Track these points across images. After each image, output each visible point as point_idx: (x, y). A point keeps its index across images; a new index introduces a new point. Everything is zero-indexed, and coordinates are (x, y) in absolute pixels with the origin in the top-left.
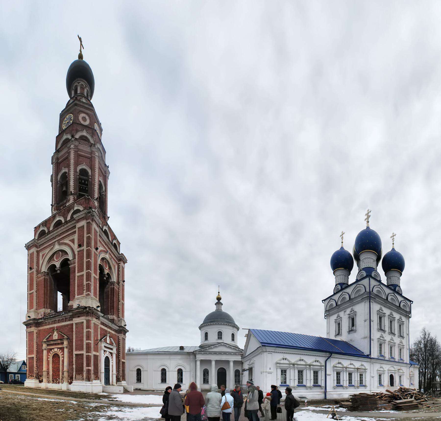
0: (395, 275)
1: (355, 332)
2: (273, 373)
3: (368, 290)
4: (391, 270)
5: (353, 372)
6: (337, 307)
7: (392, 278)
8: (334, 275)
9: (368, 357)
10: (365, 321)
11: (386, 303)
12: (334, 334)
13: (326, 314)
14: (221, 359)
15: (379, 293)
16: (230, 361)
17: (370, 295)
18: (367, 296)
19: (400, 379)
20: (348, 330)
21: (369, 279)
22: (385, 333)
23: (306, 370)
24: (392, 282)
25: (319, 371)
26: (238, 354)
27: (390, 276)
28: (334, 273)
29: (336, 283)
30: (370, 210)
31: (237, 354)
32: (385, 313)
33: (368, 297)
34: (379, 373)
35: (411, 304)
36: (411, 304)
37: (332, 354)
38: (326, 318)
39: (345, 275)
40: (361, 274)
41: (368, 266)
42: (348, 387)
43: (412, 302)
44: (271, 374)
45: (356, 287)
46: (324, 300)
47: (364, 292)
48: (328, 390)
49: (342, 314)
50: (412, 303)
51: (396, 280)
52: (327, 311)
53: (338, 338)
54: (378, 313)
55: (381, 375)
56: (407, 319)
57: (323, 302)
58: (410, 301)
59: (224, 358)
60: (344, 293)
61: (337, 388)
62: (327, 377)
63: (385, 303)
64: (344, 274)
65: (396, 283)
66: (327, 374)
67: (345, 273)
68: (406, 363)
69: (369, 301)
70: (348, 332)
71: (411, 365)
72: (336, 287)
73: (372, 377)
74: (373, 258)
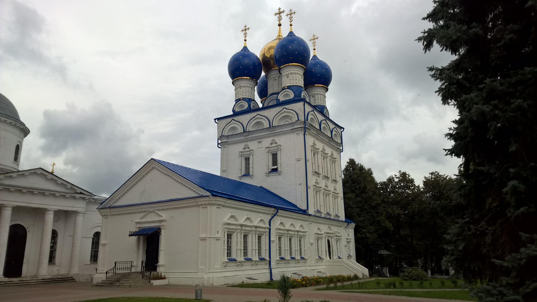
0: (318, 93)
1: (280, 174)
3: (302, 118)
4: (315, 86)
5: (293, 237)
6: (245, 134)
7: (316, 96)
8: (233, 86)
9: (304, 212)
10: (299, 160)
11: (318, 134)
13: (220, 142)
14: (29, 205)
15: (312, 122)
16: (49, 210)
17: (305, 126)
18: (300, 126)
19: (228, 241)
21: (304, 105)
22: (319, 177)
24: (317, 101)
25: (249, 235)
26: (70, 196)
27: (313, 93)
28: (233, 83)
29: (236, 97)
30: (316, 36)
31: (68, 196)
32: (328, 153)
33: (303, 129)
34: (278, 234)
35: (342, 132)
36: (342, 132)
37: (278, 210)
39: (252, 87)
43: (343, 129)
44: (205, 241)
45: (282, 112)
46: (219, 119)
47: (296, 121)
48: (272, 267)
49: (252, 145)
50: (342, 130)
51: (322, 99)
52: (224, 136)
53: (246, 180)
54: (312, 150)
55: (231, 235)
56: (338, 154)
57: (216, 121)
58: (341, 128)
59: (36, 202)
60: (258, 116)
61: (261, 263)
62: (271, 243)
63: (317, 134)
64: (251, 86)
65: (322, 103)
66: (271, 240)
67: (253, 85)
68: (341, 221)
69: (303, 133)
71: (347, 224)
72: (237, 104)
73: (201, 240)
74: (299, 73)
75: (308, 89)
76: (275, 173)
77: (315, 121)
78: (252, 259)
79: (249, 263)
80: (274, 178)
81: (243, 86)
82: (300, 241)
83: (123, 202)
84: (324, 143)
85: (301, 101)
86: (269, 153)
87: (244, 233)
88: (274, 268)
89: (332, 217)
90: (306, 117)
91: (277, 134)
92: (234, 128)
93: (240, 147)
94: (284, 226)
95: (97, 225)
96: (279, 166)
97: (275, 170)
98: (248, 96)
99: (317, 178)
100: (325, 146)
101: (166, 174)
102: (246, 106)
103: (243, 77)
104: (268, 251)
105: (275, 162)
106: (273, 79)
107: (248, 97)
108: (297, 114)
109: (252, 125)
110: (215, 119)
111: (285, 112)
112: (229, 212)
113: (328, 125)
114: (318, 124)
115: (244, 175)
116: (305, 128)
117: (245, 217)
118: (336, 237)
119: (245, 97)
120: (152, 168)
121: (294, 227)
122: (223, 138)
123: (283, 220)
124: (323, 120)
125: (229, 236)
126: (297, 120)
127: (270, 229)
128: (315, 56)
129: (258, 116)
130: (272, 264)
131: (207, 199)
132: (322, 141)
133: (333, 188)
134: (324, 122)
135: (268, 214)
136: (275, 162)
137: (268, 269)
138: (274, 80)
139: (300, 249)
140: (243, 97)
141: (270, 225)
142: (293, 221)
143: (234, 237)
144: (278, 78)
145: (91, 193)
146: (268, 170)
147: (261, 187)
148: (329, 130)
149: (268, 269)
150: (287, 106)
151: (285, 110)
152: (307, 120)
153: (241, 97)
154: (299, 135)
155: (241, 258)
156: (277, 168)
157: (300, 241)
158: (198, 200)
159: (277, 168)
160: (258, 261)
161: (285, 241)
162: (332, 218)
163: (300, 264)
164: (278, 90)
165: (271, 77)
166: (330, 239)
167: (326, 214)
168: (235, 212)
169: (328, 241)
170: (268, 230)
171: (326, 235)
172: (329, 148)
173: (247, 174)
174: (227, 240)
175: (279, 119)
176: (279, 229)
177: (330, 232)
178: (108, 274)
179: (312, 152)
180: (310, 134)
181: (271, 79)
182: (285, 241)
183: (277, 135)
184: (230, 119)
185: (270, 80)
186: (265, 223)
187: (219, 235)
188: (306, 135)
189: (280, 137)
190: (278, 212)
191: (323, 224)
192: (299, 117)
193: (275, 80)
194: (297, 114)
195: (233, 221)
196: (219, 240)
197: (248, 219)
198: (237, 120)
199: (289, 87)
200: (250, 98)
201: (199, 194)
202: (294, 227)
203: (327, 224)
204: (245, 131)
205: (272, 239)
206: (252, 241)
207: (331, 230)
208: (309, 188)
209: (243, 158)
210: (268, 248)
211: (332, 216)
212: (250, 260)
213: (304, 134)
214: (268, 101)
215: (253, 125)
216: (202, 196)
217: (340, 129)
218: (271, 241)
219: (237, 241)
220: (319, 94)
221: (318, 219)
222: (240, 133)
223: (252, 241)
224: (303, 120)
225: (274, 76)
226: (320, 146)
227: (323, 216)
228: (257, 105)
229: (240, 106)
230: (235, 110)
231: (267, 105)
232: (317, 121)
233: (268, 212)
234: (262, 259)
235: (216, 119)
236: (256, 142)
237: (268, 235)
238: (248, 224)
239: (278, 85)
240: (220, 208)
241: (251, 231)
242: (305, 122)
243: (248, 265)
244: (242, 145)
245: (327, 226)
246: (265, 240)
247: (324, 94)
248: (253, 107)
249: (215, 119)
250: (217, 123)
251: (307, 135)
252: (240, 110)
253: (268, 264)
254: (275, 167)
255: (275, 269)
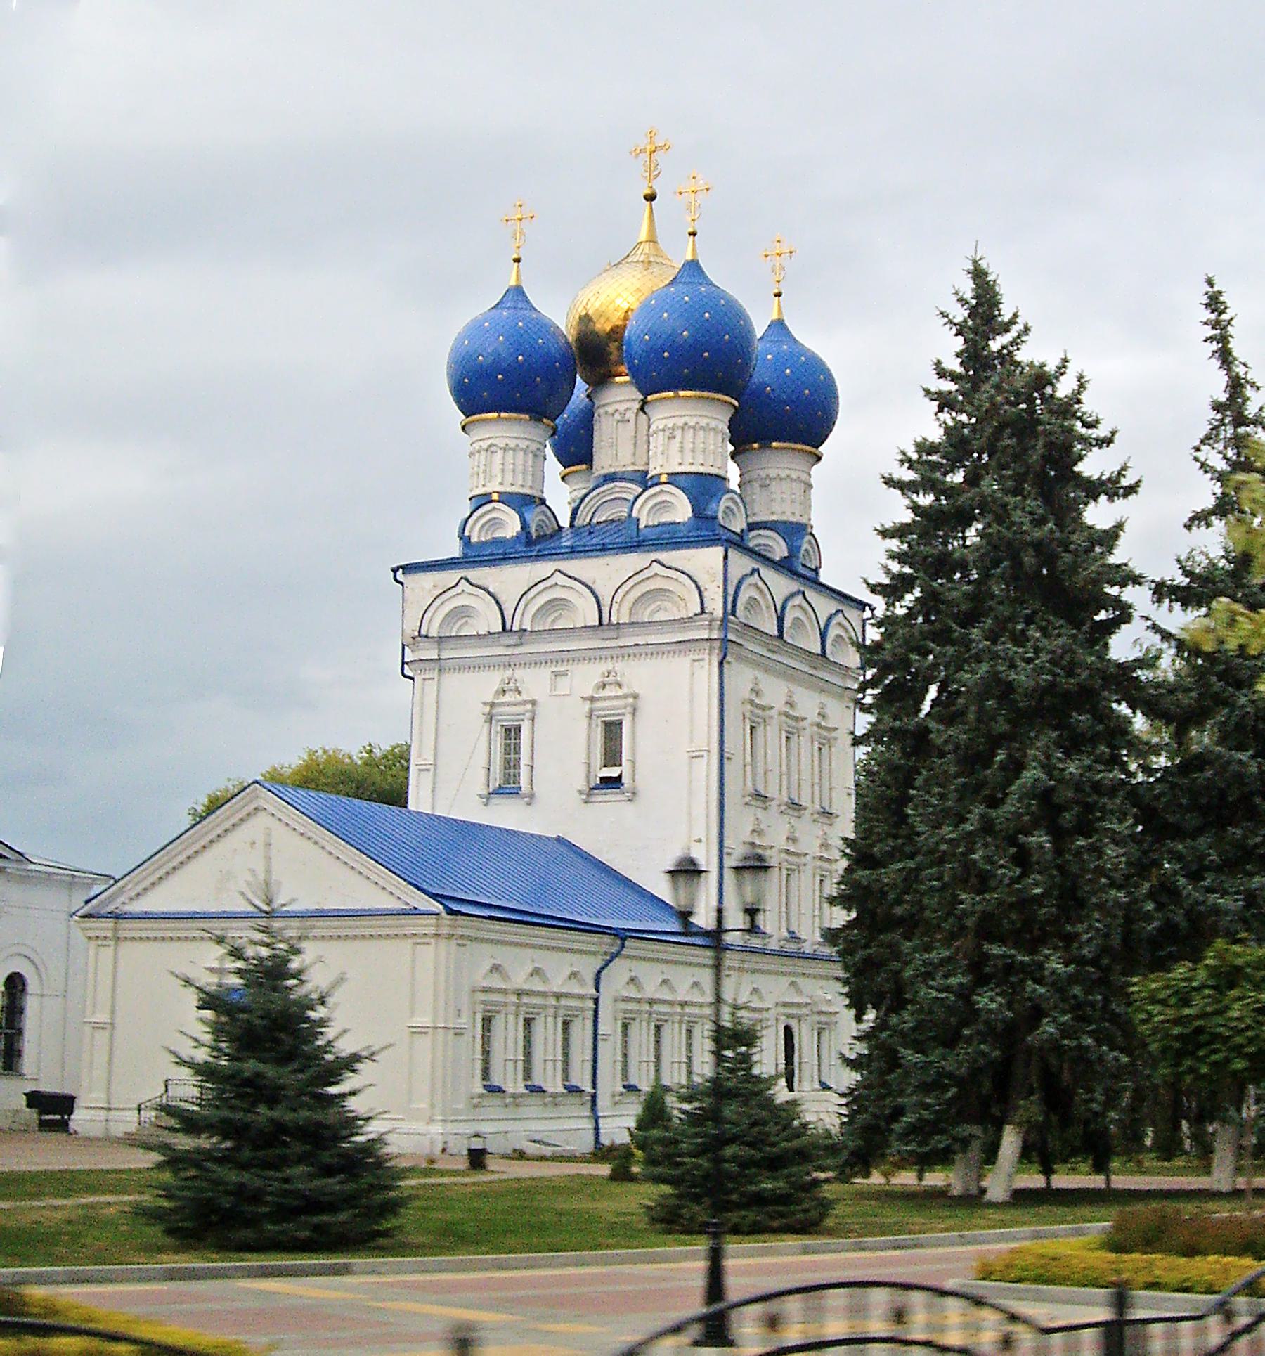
2: (611, 1038)
12: (478, 786)
18: (705, 634)
20: (581, 784)
22: (765, 809)
23: (583, 1019)
27: (763, 474)
33: (717, 644)
34: (621, 1015)
37: (623, 939)
38: (407, 671)
40: (659, 499)
41: (701, 470)
42: (522, 1095)
45: (646, 574)
47: (696, 615)
49: (535, 682)
53: (506, 816)
54: (748, 715)
62: (600, 1044)
64: (534, 446)
70: (581, 792)
75: (748, 455)
76: (611, 795)
77: (764, 607)
78: (545, 1089)
79: (535, 1099)
80: (609, 805)
81: (503, 446)
82: (689, 1031)
83: (153, 903)
84: (791, 679)
85: (717, 545)
86: (594, 717)
87: (527, 1013)
88: (605, 1117)
89: (808, 948)
90: (730, 599)
91: (625, 651)
92: (461, 613)
93: (486, 684)
94: (640, 987)
95: (32, 956)
96: (625, 770)
97: (612, 783)
98: (522, 486)
99: (760, 813)
100: (793, 688)
101: (302, 834)
102: (511, 525)
103: (682, 393)
104: (588, 1066)
105: (612, 756)
106: (617, 416)
107: (522, 491)
108: (698, 587)
109: (533, 608)
110: (395, 571)
111: (656, 574)
112: (485, 956)
113: (813, 608)
114: (774, 614)
115: (499, 792)
116: (725, 641)
117: (529, 969)
118: (816, 1018)
119: (509, 489)
120: (256, 809)
121: (672, 989)
122: (424, 644)
123: (640, 969)
124: (793, 595)
125: (487, 1022)
126: (698, 610)
127: (596, 1001)
128: (779, 326)
129: (559, 578)
130: (600, 1103)
131: (432, 920)
132: (788, 674)
133: (819, 842)
134: (798, 600)
135: (594, 953)
136: (612, 756)
137: (589, 1117)
138: (619, 421)
139: (689, 1058)
140: (502, 489)
141: (597, 990)
142: (670, 972)
143: (498, 1023)
144: (634, 416)
145: (21, 854)
146: (588, 782)
147: (559, 840)
148: (813, 630)
149: (589, 1117)
150: (663, 556)
151: (656, 568)
152: (733, 614)
153: (494, 487)
154: (701, 663)
155: (515, 1085)
156: (620, 776)
157: (689, 1031)
158: (404, 920)
159: (620, 776)
160: (562, 1095)
161: (642, 1036)
162: (807, 951)
163: (521, 1109)
164: (633, 464)
165: (610, 409)
166: (794, 1024)
167: (786, 940)
168: (502, 955)
169: (788, 1030)
170: (591, 1004)
171: (781, 1010)
172: (811, 693)
173: (508, 787)
174: (480, 1032)
175: (633, 600)
176: (626, 999)
177: (797, 999)
178: (142, 1112)
179: (747, 721)
180: (739, 658)
181: (606, 412)
182: (642, 1036)
183: (623, 653)
184: (451, 576)
185: (603, 419)
186: (582, 982)
187: (464, 1021)
188: (725, 665)
189: (633, 663)
190: (623, 946)
191: (770, 972)
192: (705, 599)
193: (622, 421)
194: (698, 587)
195: (496, 982)
196: (462, 1034)
197: (536, 972)
198: (479, 583)
199: (674, 478)
200: (528, 492)
201: (407, 904)
202: (672, 989)
203: (784, 974)
204: (508, 627)
205: (602, 1029)
206: (547, 1035)
207: (799, 991)
208: (729, 854)
209: (497, 728)
210: (588, 1056)
211: (771, 940)
212: (540, 1090)
213: (721, 664)
214: (593, 502)
215: (538, 610)
216: (415, 912)
217: (859, 612)
218: (599, 1037)
219: (508, 1034)
220: (788, 480)
221: (755, 958)
222: (490, 633)
223: (547, 1035)
224: (719, 613)
225: (622, 407)
226: (775, 692)
227: (773, 945)
228: (553, 519)
229: (486, 527)
230: (469, 537)
231: (588, 520)
232: (768, 607)
233: (593, 948)
234: (573, 1090)
235: (398, 568)
236: (545, 672)
237: (592, 1018)
238: (535, 989)
239: (635, 444)
240: (464, 945)
241: (544, 1007)
242: (724, 620)
243: (533, 1107)
244: (495, 679)
245: (785, 980)
246: (581, 1033)
247: (804, 477)
248: (538, 525)
249: (395, 571)
250: (402, 584)
251: (729, 663)
252: (489, 538)
253: (589, 1105)
254: (613, 772)
255: (609, 1120)
